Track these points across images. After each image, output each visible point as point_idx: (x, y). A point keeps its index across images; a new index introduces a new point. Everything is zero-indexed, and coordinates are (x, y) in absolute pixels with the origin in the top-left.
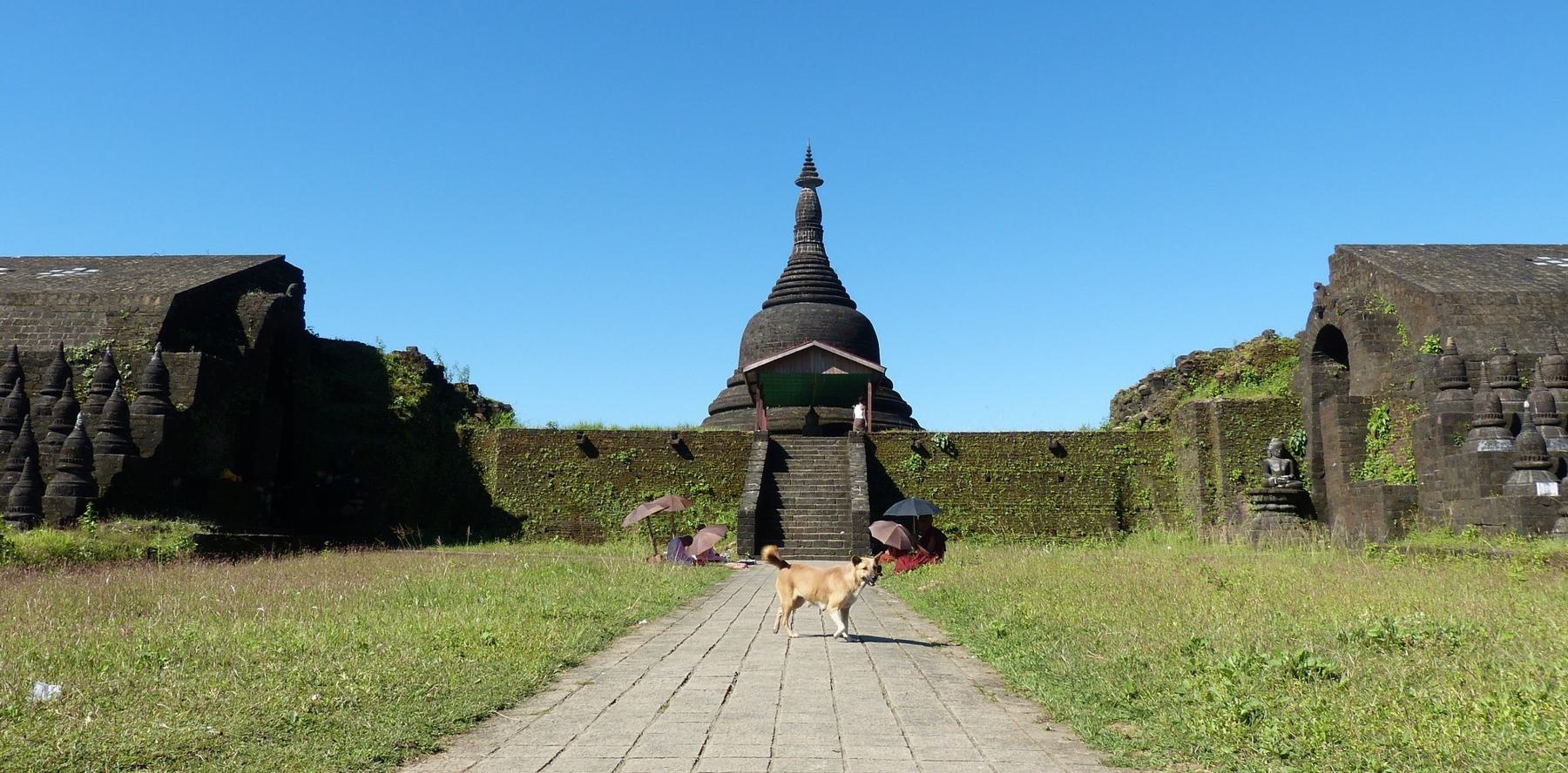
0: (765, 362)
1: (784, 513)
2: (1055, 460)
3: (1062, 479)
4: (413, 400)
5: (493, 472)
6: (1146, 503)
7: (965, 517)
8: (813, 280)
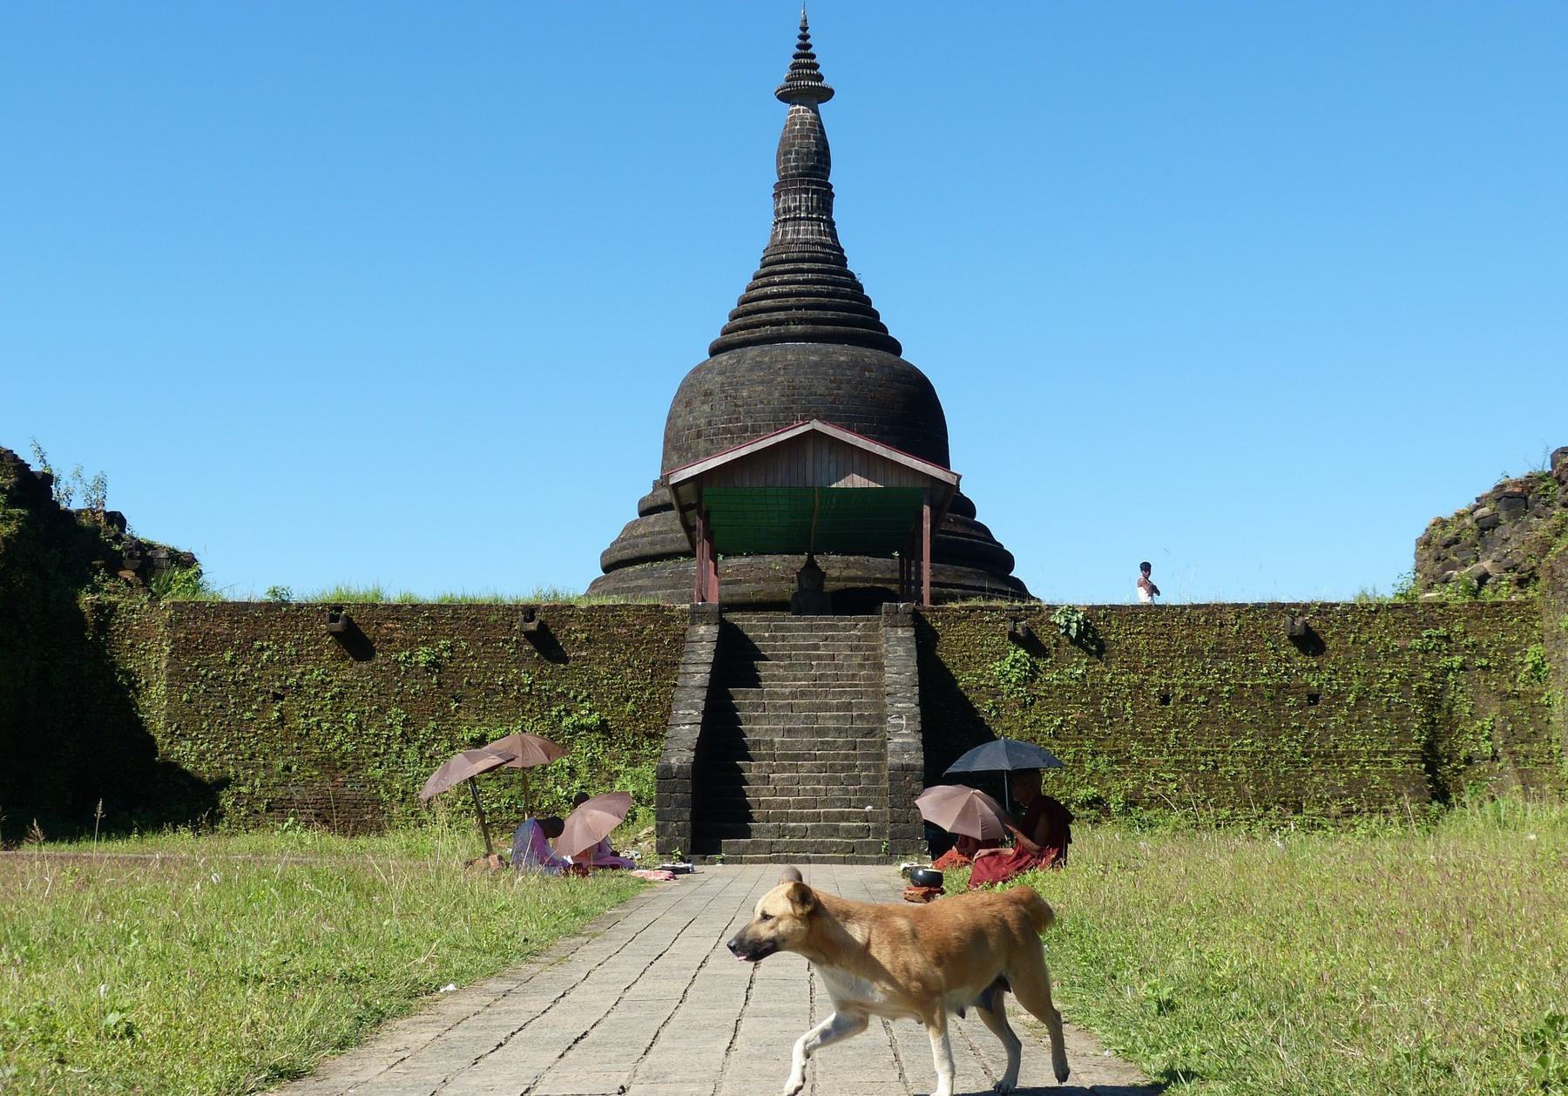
0: (744, 451)
1: (751, 770)
2: (1300, 661)
3: (1314, 698)
5: (159, 689)
6: (1486, 747)
7: (1119, 777)
8: (814, 300)
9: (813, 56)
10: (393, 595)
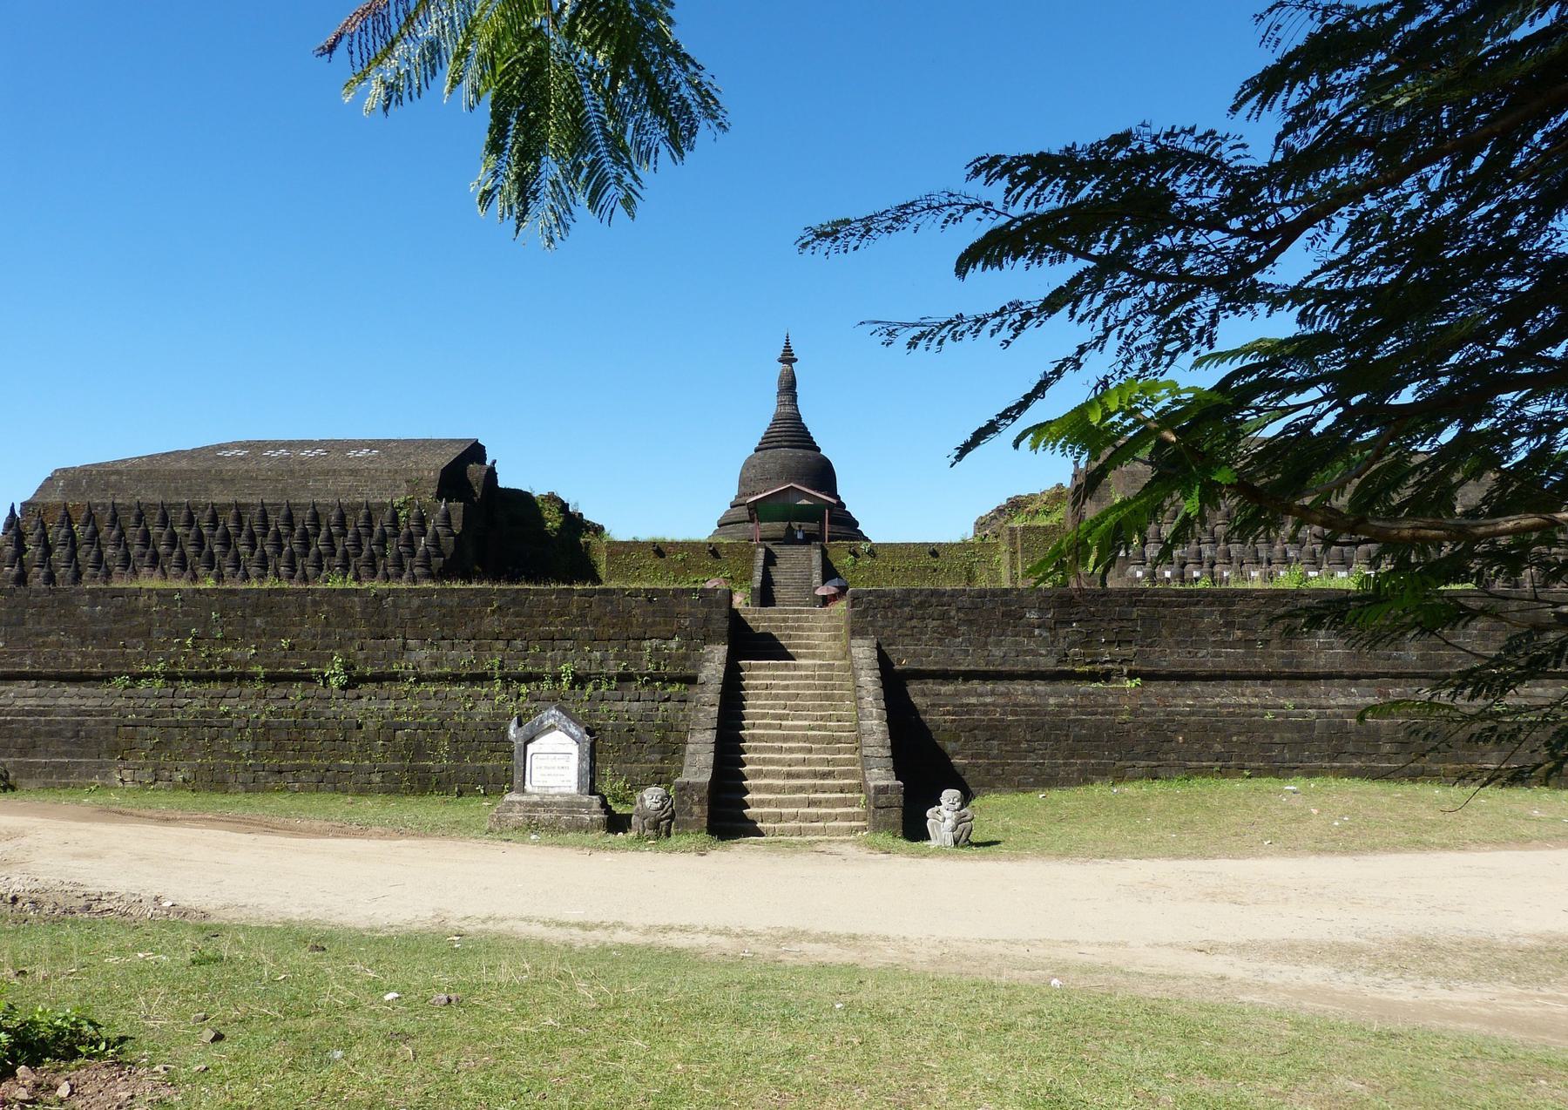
1: (775, 589)
4: (557, 525)
5: (603, 566)
8: (790, 433)
10: (669, 539)
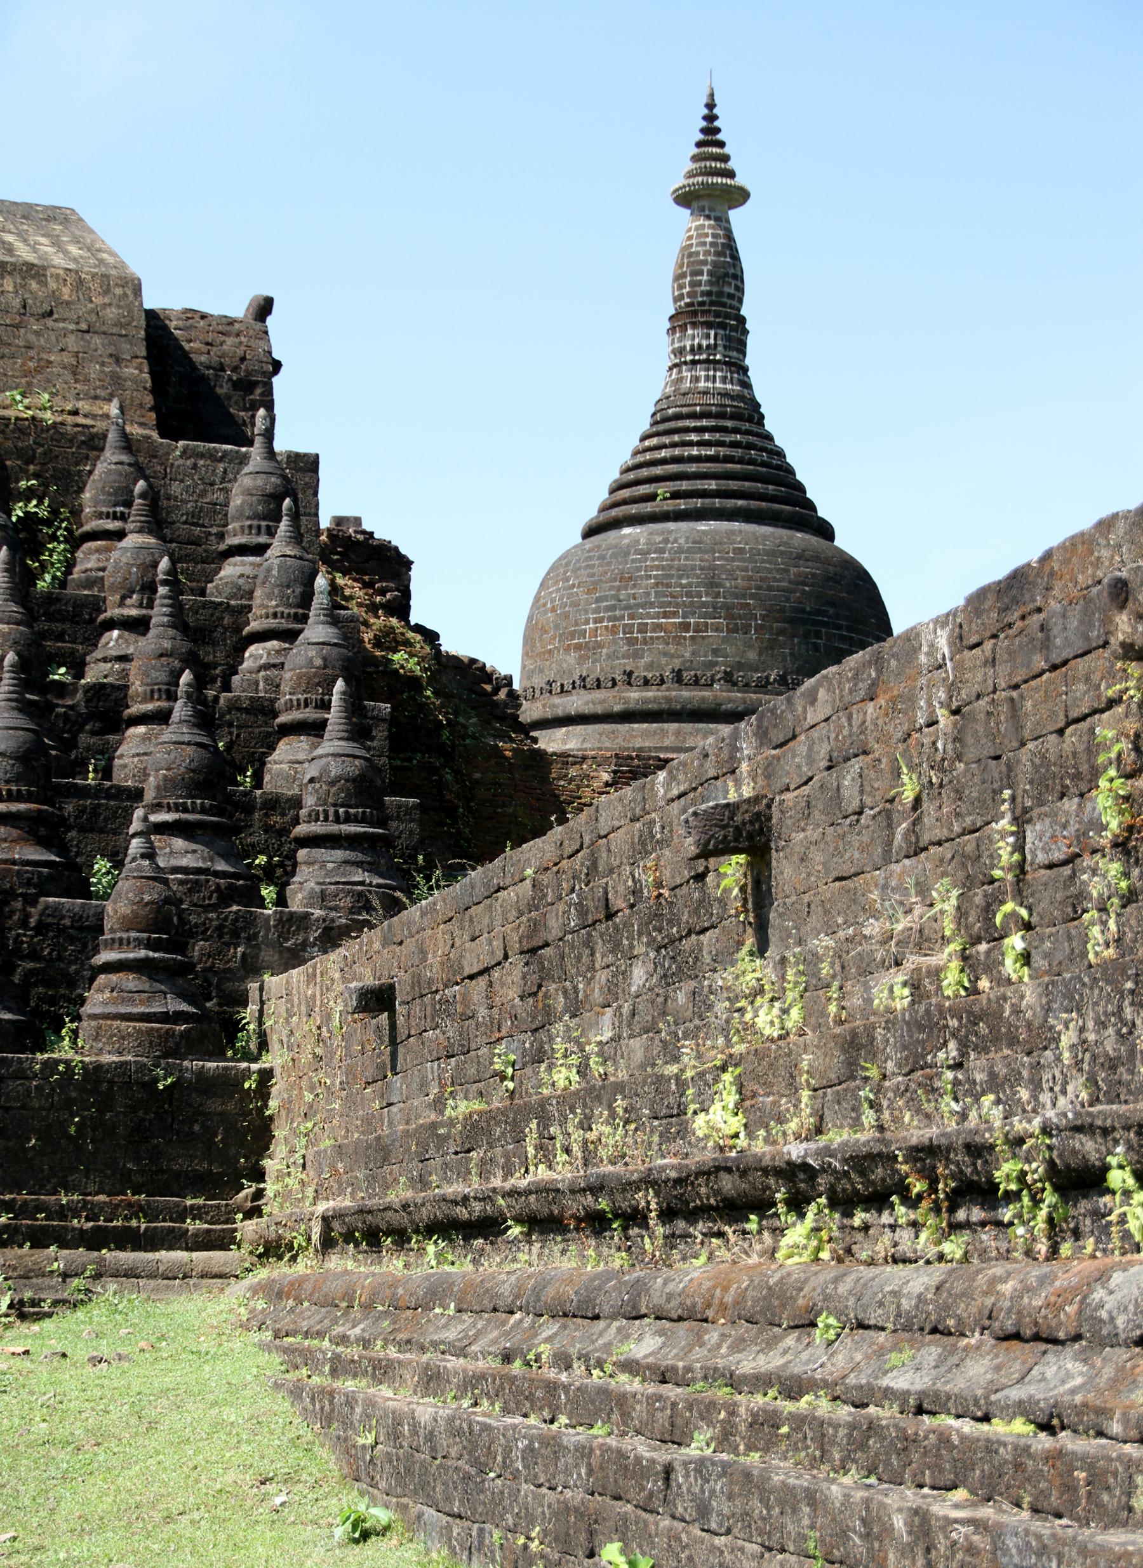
9: (721, 144)
